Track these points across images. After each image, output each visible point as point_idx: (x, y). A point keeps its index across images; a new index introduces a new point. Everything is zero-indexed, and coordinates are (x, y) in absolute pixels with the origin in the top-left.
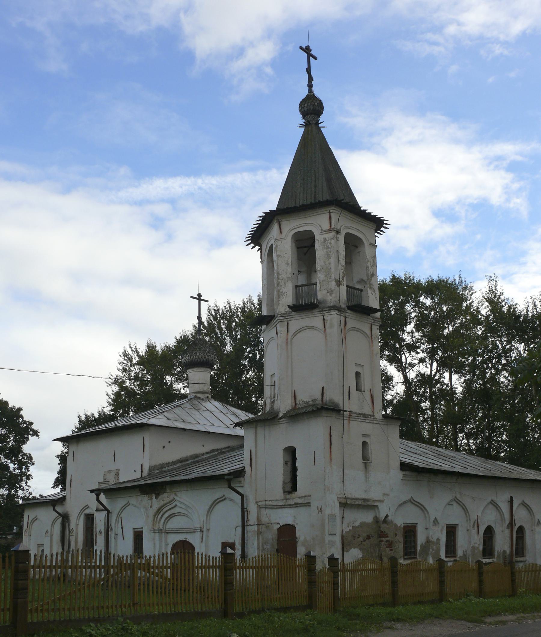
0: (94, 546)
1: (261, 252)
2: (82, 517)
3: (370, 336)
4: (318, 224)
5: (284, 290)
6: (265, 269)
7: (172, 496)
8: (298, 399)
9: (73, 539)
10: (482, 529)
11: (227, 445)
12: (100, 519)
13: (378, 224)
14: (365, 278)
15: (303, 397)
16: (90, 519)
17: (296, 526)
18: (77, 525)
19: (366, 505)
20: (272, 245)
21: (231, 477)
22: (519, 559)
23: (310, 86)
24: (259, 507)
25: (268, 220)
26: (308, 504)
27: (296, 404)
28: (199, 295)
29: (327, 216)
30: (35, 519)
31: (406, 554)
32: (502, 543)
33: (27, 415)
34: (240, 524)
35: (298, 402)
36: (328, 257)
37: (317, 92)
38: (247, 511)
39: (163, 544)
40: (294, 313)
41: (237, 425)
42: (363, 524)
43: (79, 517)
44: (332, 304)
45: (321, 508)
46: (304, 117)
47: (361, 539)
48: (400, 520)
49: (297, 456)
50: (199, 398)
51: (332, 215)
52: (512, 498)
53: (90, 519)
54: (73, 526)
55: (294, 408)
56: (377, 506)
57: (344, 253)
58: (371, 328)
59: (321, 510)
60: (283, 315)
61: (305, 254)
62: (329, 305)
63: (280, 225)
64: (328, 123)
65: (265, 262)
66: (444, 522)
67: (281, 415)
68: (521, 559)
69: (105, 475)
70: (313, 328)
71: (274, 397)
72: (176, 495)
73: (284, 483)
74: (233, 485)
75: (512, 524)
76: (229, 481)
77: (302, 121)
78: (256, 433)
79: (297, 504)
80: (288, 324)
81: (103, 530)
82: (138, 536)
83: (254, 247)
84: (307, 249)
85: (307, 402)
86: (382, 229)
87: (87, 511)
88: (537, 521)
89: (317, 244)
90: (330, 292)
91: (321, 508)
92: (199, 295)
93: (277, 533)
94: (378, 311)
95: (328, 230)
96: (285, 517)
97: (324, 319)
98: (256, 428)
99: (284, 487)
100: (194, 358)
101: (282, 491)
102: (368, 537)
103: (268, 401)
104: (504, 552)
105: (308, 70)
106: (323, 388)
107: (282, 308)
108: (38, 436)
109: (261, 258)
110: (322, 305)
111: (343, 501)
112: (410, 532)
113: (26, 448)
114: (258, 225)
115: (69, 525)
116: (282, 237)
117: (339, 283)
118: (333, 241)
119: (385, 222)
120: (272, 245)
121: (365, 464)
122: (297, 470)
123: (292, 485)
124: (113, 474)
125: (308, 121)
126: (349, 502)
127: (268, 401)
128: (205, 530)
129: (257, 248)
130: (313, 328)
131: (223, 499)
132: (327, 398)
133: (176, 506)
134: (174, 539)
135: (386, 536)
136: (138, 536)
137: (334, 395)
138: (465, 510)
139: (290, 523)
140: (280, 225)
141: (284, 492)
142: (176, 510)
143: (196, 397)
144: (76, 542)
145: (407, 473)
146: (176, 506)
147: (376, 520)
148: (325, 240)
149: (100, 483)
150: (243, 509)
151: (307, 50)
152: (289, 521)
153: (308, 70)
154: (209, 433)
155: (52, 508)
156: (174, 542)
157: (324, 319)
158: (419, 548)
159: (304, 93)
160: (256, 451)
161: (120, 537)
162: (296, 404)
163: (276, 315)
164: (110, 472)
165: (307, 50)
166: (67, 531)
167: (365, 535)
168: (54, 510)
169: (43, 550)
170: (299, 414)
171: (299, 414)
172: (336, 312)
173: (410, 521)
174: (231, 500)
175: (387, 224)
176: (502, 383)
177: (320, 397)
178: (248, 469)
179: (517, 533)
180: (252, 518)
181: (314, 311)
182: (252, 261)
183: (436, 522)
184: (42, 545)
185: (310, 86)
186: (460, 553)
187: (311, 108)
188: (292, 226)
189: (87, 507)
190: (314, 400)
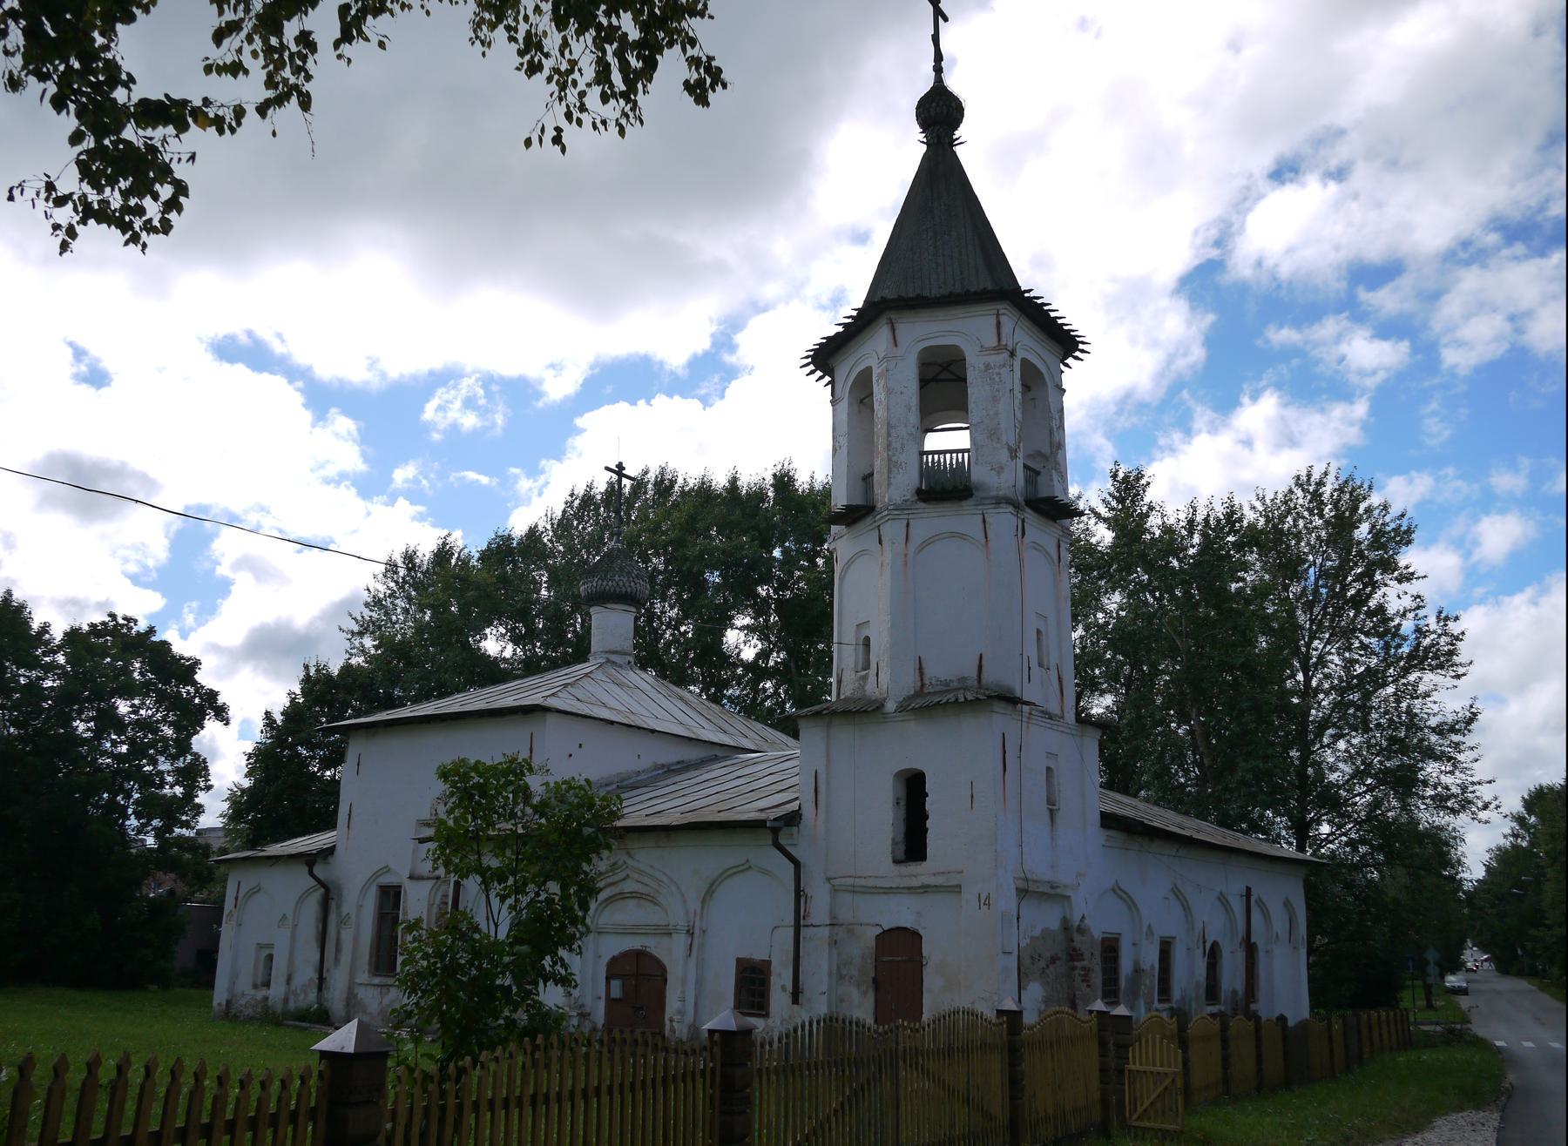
4: (971, 332)
6: (844, 416)
7: (621, 857)
8: (928, 673)
9: (347, 935)
10: (1208, 946)
11: (679, 758)
13: (1066, 343)
14: (1046, 450)
15: (942, 669)
17: (922, 932)
18: (360, 907)
19: (1052, 894)
23: (938, 70)
24: (835, 890)
26: (956, 889)
27: (923, 685)
28: (620, 466)
29: (993, 320)
30: (256, 890)
32: (1232, 978)
34: (790, 919)
35: (927, 682)
36: (995, 399)
37: (953, 83)
40: (922, 505)
42: (1046, 932)
43: (365, 889)
44: (1001, 493)
45: (988, 897)
47: (1042, 964)
48: (1098, 928)
50: (614, 663)
51: (1003, 319)
52: (1249, 890)
54: (348, 907)
55: (920, 693)
56: (1068, 897)
59: (987, 903)
62: (994, 493)
63: (893, 330)
64: (974, 148)
65: (844, 404)
66: (1162, 931)
67: (890, 706)
70: (962, 536)
72: (628, 854)
73: (894, 843)
74: (782, 841)
76: (775, 831)
79: (928, 886)
83: (812, 372)
85: (946, 683)
86: (1070, 361)
87: (387, 880)
88: (1145, 929)
89: (971, 375)
90: (1000, 470)
91: (988, 897)
92: (620, 466)
93: (873, 943)
95: (994, 349)
99: (893, 852)
100: (609, 585)
101: (890, 859)
102: (1053, 960)
104: (1234, 992)
105: (936, 39)
111: (1021, 885)
112: (1110, 949)
113: (200, 742)
115: (339, 907)
116: (893, 359)
117: (1013, 454)
118: (1003, 371)
119: (819, 373)
123: (913, 845)
125: (938, 137)
126: (1032, 887)
128: (697, 931)
129: (827, 379)
130: (962, 536)
131: (746, 868)
132: (987, 677)
133: (627, 876)
137: (999, 674)
138: (1187, 909)
140: (893, 330)
142: (629, 886)
143: (608, 661)
144: (356, 940)
145: (1110, 833)
146: (627, 876)
147: (1066, 925)
148: (988, 367)
150: (798, 892)
152: (907, 921)
153: (936, 39)
154: (653, 731)
155: (306, 869)
156: (616, 953)
158: (1123, 983)
159: (925, 84)
162: (923, 685)
163: (879, 505)
166: (333, 918)
167: (1048, 955)
168: (311, 874)
169: (270, 957)
170: (933, 702)
171: (933, 702)
172: (1011, 509)
173: (1113, 929)
174: (764, 871)
175: (1083, 351)
177: (974, 674)
178: (809, 811)
180: (819, 908)
181: (964, 503)
182: (815, 400)
184: (271, 946)
185: (938, 70)
186: (1176, 994)
187: (940, 113)
190: (962, 679)
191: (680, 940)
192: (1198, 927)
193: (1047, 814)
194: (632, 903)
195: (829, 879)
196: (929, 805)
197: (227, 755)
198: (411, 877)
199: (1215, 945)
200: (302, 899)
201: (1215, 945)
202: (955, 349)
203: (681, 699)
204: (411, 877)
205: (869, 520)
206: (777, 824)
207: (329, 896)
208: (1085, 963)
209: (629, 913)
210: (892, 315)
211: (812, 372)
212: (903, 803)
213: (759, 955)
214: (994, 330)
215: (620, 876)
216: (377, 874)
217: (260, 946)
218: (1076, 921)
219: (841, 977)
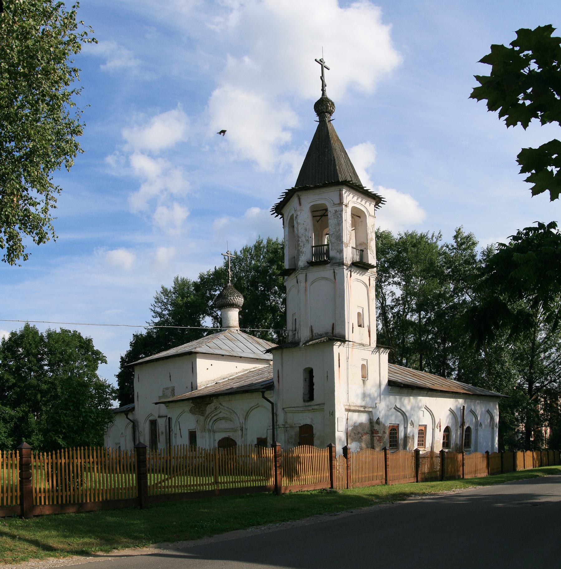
0: (158, 444)
1: (283, 220)
2: (148, 422)
3: (368, 285)
4: (323, 197)
5: (304, 250)
6: (287, 233)
10: (443, 428)
12: (162, 423)
16: (153, 423)
20: (293, 215)
21: (264, 390)
22: (466, 449)
25: (289, 195)
27: (313, 336)
31: (390, 446)
33: (97, 346)
35: (314, 335)
38: (276, 415)
39: (212, 440)
41: (268, 351)
46: (318, 115)
49: (314, 374)
53: (153, 423)
57: (350, 222)
58: (369, 280)
60: (302, 269)
61: (318, 222)
62: (338, 261)
63: (299, 199)
65: (287, 229)
68: (468, 449)
69: (163, 391)
70: (326, 279)
71: (295, 330)
73: (304, 394)
74: (266, 396)
75: (463, 424)
76: (263, 393)
77: (317, 119)
78: (282, 358)
80: (306, 275)
81: (164, 431)
82: (193, 436)
83: (277, 216)
84: (319, 218)
86: (380, 204)
94: (375, 267)
96: (305, 419)
97: (334, 272)
98: (282, 353)
99: (303, 398)
103: (291, 333)
105: (322, 78)
106: (333, 324)
107: (302, 262)
108: (106, 363)
109: (283, 225)
110: (334, 261)
114: (282, 199)
119: (276, 214)
120: (293, 215)
121: (364, 381)
122: (313, 385)
124: (170, 390)
127: (291, 333)
129: (280, 216)
130: (326, 279)
131: (257, 406)
133: (221, 412)
134: (219, 436)
135: (377, 432)
136: (193, 436)
139: (309, 423)
140: (299, 199)
141: (304, 401)
142: (221, 415)
147: (371, 421)
149: (160, 397)
151: (321, 62)
152: (308, 422)
153: (322, 78)
154: (241, 357)
157: (334, 272)
159: (319, 96)
160: (282, 371)
161: (178, 436)
162: (313, 336)
164: (167, 389)
165: (321, 62)
169: (120, 447)
175: (383, 201)
176: (519, 300)
177: (331, 331)
178: (276, 383)
179: (466, 432)
180: (281, 420)
181: (326, 266)
183: (412, 424)
184: (119, 443)
188: (310, 200)
189: (151, 415)
191: (240, 432)
192: (437, 421)
193: (362, 381)
194: (223, 421)
195: (283, 409)
196: (315, 380)
197: (108, 373)
198: (159, 417)
199: (469, 429)
200: (127, 426)
201: (469, 429)
202: (323, 205)
203: (258, 343)
204: (159, 417)
205: (293, 275)
206: (264, 390)
207: (135, 425)
208: (380, 435)
209: (223, 425)
210: (299, 193)
211: (277, 216)
212: (307, 380)
213: (264, 437)
214: (338, 197)
215: (218, 412)
216: (148, 416)
217: (117, 444)
218: (375, 419)
219: (289, 442)
